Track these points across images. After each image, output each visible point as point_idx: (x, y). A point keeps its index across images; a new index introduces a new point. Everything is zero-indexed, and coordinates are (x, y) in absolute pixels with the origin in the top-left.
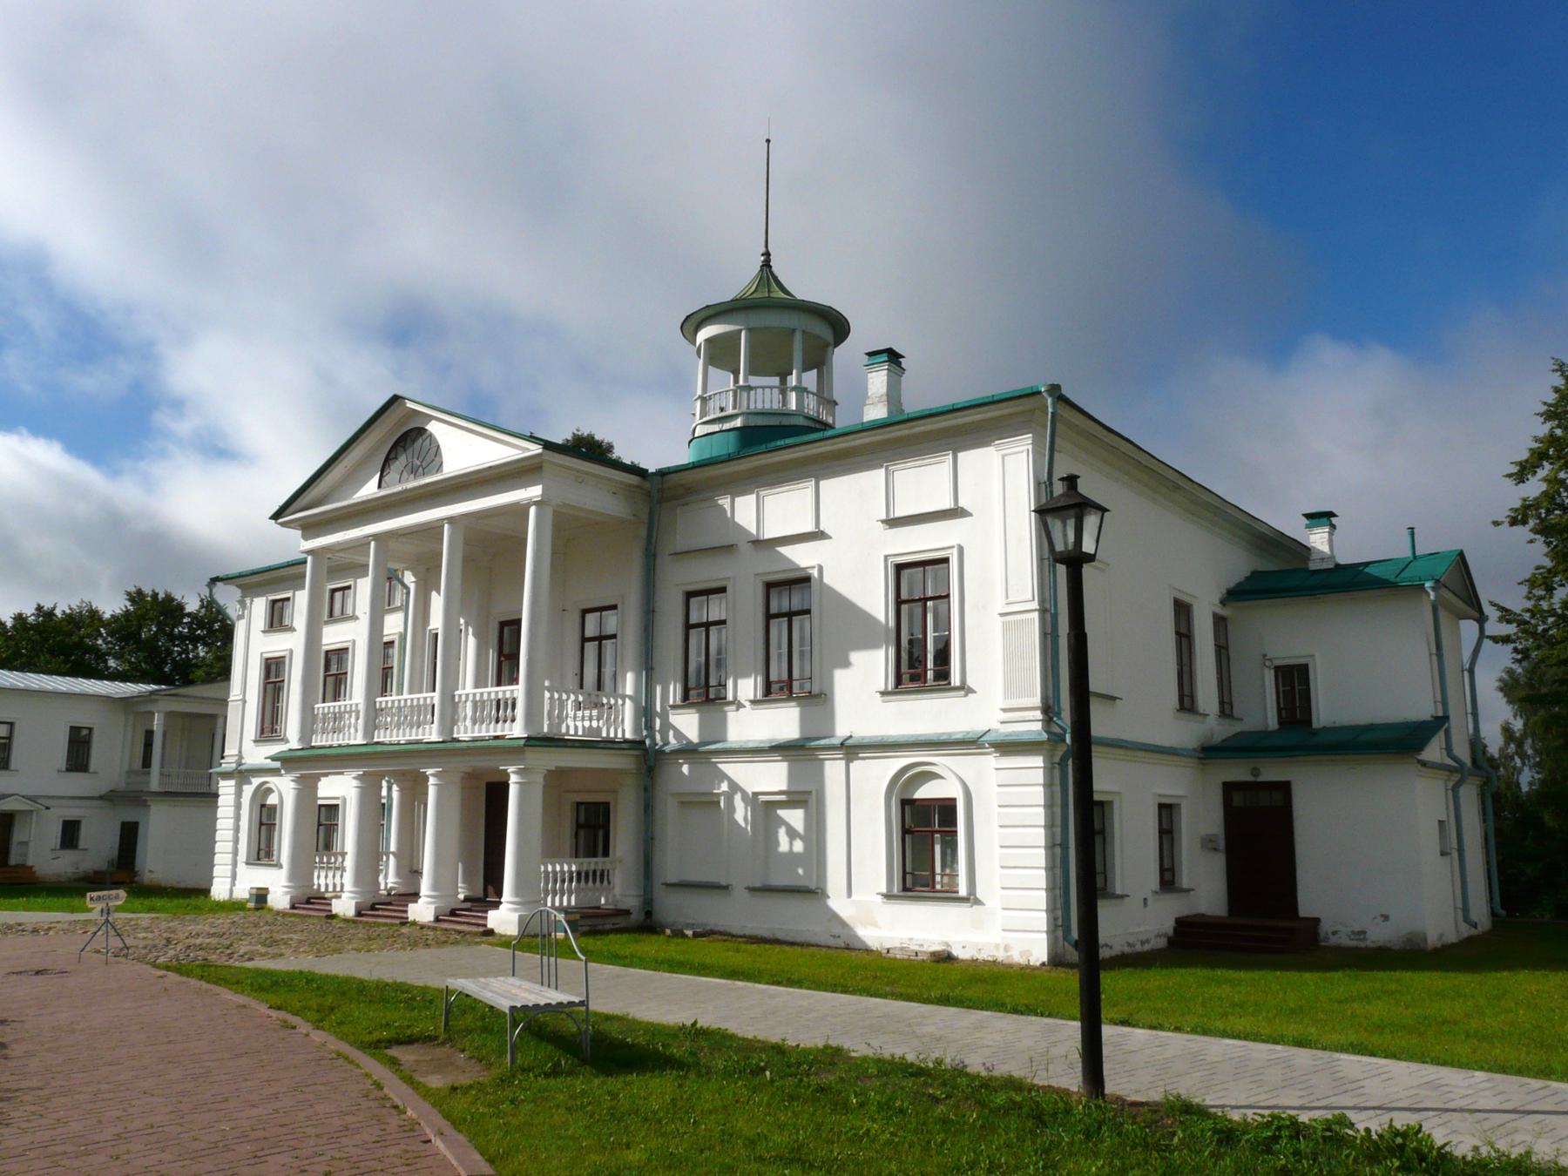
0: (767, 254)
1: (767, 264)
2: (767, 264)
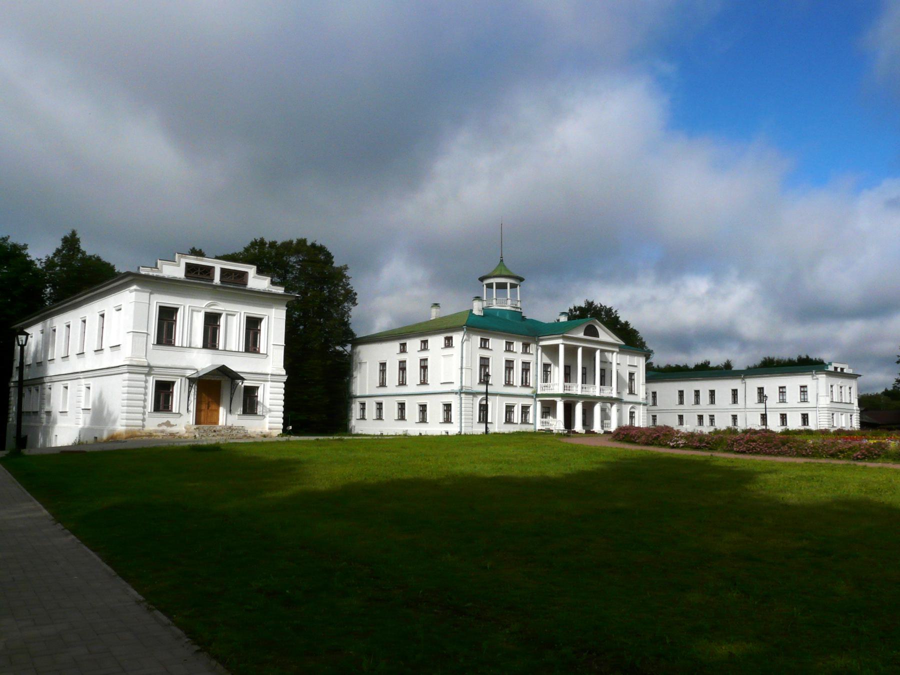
1: (502, 261)
2: (502, 261)
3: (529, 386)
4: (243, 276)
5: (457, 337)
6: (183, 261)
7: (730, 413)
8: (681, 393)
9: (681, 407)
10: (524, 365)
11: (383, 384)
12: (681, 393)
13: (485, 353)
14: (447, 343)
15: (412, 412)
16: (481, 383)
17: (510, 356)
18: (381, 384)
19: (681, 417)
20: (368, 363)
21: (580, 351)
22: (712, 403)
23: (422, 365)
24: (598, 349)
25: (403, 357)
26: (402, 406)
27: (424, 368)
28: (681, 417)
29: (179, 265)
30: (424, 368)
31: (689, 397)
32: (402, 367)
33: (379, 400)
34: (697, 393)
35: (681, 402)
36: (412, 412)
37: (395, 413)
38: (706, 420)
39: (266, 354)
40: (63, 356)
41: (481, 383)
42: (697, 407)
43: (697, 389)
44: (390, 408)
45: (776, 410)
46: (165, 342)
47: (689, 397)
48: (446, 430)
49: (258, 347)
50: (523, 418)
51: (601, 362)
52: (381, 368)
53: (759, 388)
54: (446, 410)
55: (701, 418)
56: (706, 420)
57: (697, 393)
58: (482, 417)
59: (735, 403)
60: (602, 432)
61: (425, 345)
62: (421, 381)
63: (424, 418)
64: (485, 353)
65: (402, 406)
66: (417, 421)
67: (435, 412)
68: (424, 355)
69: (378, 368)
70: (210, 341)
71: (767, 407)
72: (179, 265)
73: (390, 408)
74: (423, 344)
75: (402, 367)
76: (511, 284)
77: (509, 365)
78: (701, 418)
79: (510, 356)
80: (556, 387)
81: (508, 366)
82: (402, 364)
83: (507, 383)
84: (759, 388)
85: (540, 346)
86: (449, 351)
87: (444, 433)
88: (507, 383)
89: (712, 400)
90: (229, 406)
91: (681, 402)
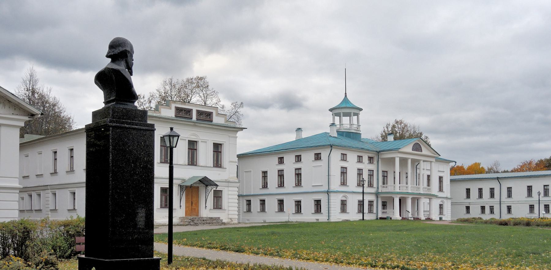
0: (346, 93)
3: (373, 187)
4: (210, 115)
5: (324, 154)
6: (173, 106)
7: (506, 204)
8: (468, 191)
9: (468, 200)
10: (369, 171)
11: (265, 186)
12: (468, 191)
13: (344, 164)
14: (316, 157)
15: (290, 206)
16: (359, 185)
17: (360, 166)
18: (263, 187)
19: (468, 208)
20: (252, 172)
21: (410, 161)
22: (492, 197)
23: (297, 173)
24: (409, 158)
25: (281, 167)
26: (281, 202)
27: (298, 175)
28: (468, 208)
29: (170, 109)
30: (298, 175)
31: (474, 193)
32: (281, 175)
33: (262, 198)
34: (480, 190)
35: (468, 196)
36: (290, 206)
37: (276, 207)
38: (487, 210)
39: (430, 170)
40: (51, 172)
41: (359, 185)
42: (481, 200)
43: (480, 187)
44: (272, 204)
45: (527, 202)
46: (164, 161)
47: (474, 193)
48: (317, 218)
49: (220, 163)
50: (215, 204)
51: (523, 171)
52: (263, 175)
53: (528, 187)
54: (280, 204)
55: (483, 208)
56: (487, 210)
57: (480, 190)
58: (300, 210)
59: (481, 198)
60: (401, 218)
61: (281, 160)
62: (278, 185)
63: (249, 209)
64: (344, 164)
65: (281, 202)
66: (313, 213)
67: (308, 205)
68: (298, 165)
69: (261, 175)
70: (192, 161)
71: (540, 200)
72: (170, 109)
73: (272, 204)
74: (297, 158)
75: (281, 175)
76: (354, 113)
77: (360, 172)
78: (483, 208)
79: (360, 166)
80: (389, 188)
81: (359, 173)
82: (280, 172)
83: (358, 184)
84: (528, 187)
85: (380, 158)
86: (318, 163)
87: (315, 221)
88: (342, 183)
89: (468, 196)
90: (180, 203)
91: (468, 196)
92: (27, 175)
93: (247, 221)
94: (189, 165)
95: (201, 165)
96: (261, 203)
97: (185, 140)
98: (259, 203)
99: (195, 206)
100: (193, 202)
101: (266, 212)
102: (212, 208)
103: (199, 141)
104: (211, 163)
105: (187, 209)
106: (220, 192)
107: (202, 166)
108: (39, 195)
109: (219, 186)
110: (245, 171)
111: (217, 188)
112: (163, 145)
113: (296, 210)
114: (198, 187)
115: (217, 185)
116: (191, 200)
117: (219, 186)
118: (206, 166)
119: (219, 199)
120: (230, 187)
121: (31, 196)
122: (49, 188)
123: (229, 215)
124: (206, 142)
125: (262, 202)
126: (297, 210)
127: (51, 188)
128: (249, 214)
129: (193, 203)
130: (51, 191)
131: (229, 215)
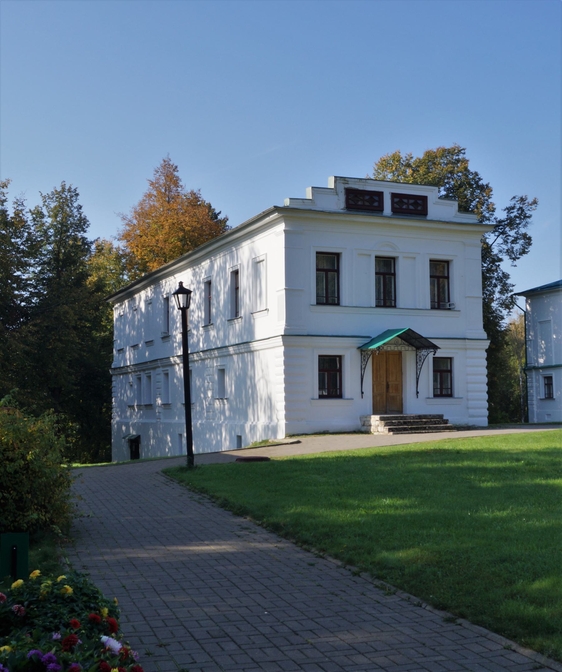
71: (528, 363)
90: (416, 386)
92: (151, 340)
93: (546, 416)
94: (433, 308)
95: (401, 307)
96: (546, 383)
97: (370, 255)
98: (542, 382)
99: (394, 391)
100: (390, 383)
101: (554, 399)
102: (431, 395)
103: (398, 257)
104: (425, 300)
105: (378, 398)
106: (449, 360)
107: (345, 306)
108: (149, 377)
109: (439, 348)
110: (539, 322)
111: (435, 352)
112: (382, 271)
113: (546, 393)
114: (400, 353)
115: (435, 348)
116: (385, 380)
117: (439, 348)
118: (425, 308)
119: (448, 376)
120: (470, 349)
121: (139, 379)
122: (160, 365)
123: (468, 408)
124: (414, 258)
125: (547, 381)
126: (548, 394)
127: (162, 364)
128: (549, 403)
129: (390, 386)
130: (163, 371)
131: (468, 408)
